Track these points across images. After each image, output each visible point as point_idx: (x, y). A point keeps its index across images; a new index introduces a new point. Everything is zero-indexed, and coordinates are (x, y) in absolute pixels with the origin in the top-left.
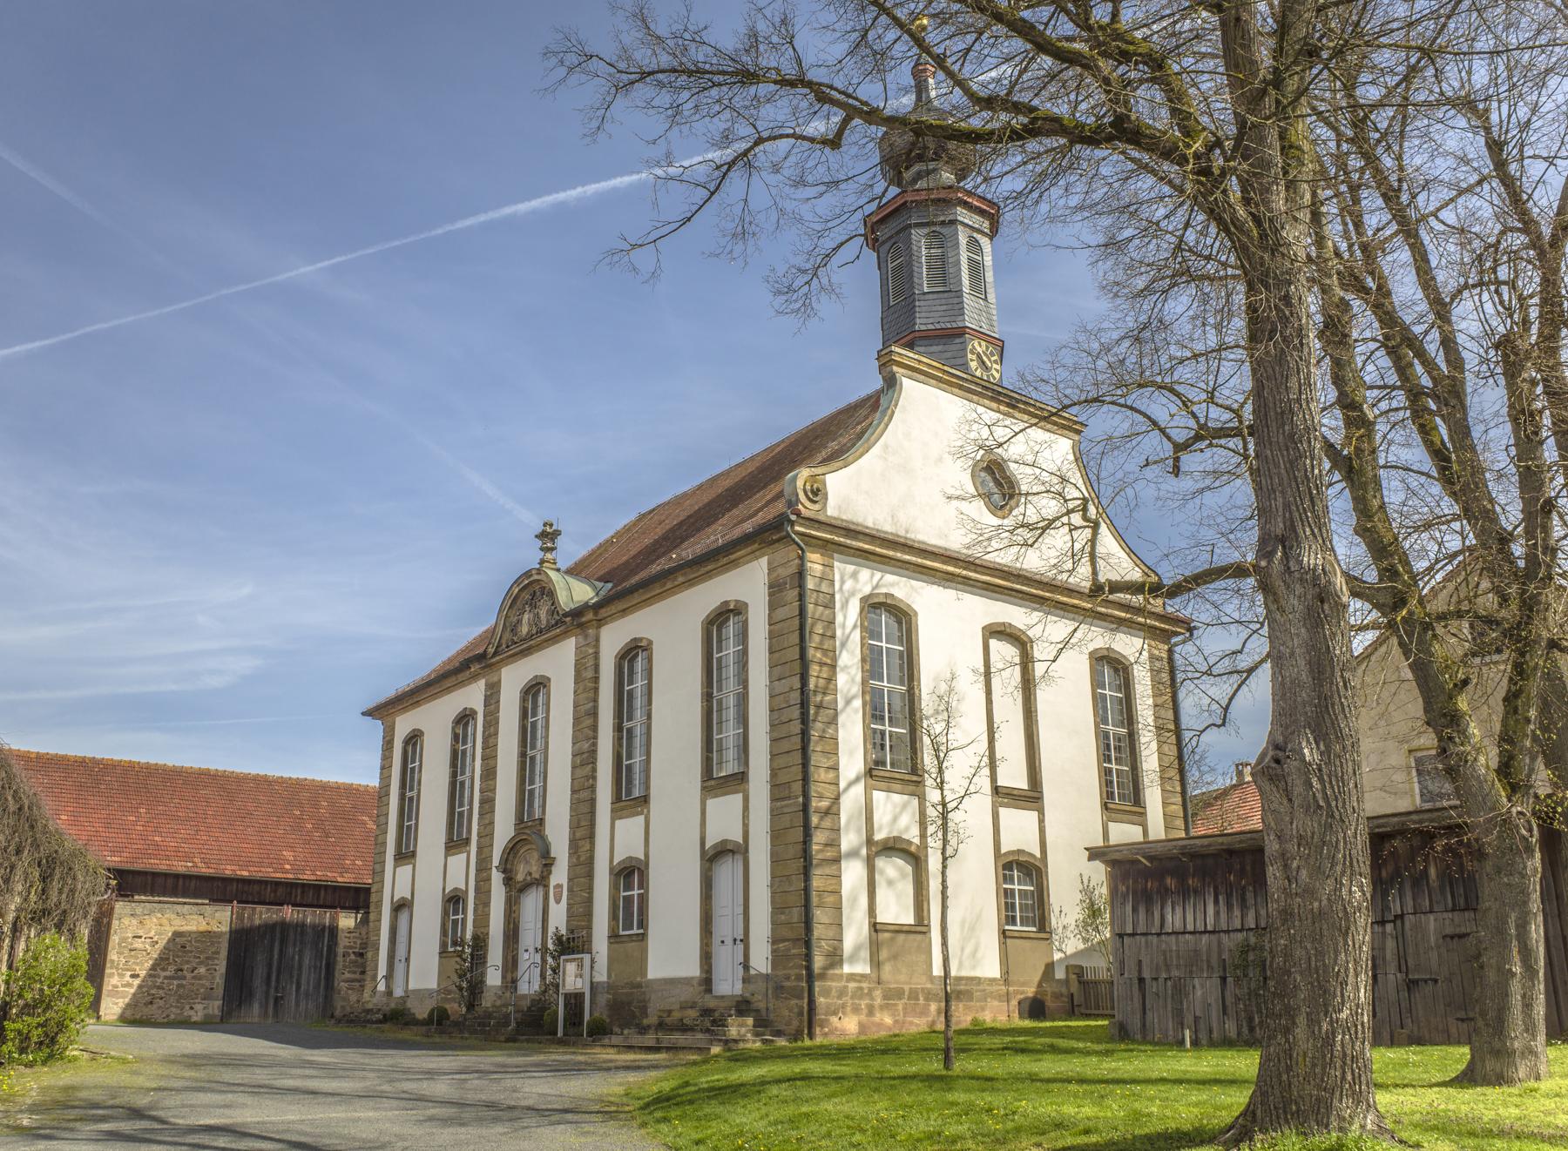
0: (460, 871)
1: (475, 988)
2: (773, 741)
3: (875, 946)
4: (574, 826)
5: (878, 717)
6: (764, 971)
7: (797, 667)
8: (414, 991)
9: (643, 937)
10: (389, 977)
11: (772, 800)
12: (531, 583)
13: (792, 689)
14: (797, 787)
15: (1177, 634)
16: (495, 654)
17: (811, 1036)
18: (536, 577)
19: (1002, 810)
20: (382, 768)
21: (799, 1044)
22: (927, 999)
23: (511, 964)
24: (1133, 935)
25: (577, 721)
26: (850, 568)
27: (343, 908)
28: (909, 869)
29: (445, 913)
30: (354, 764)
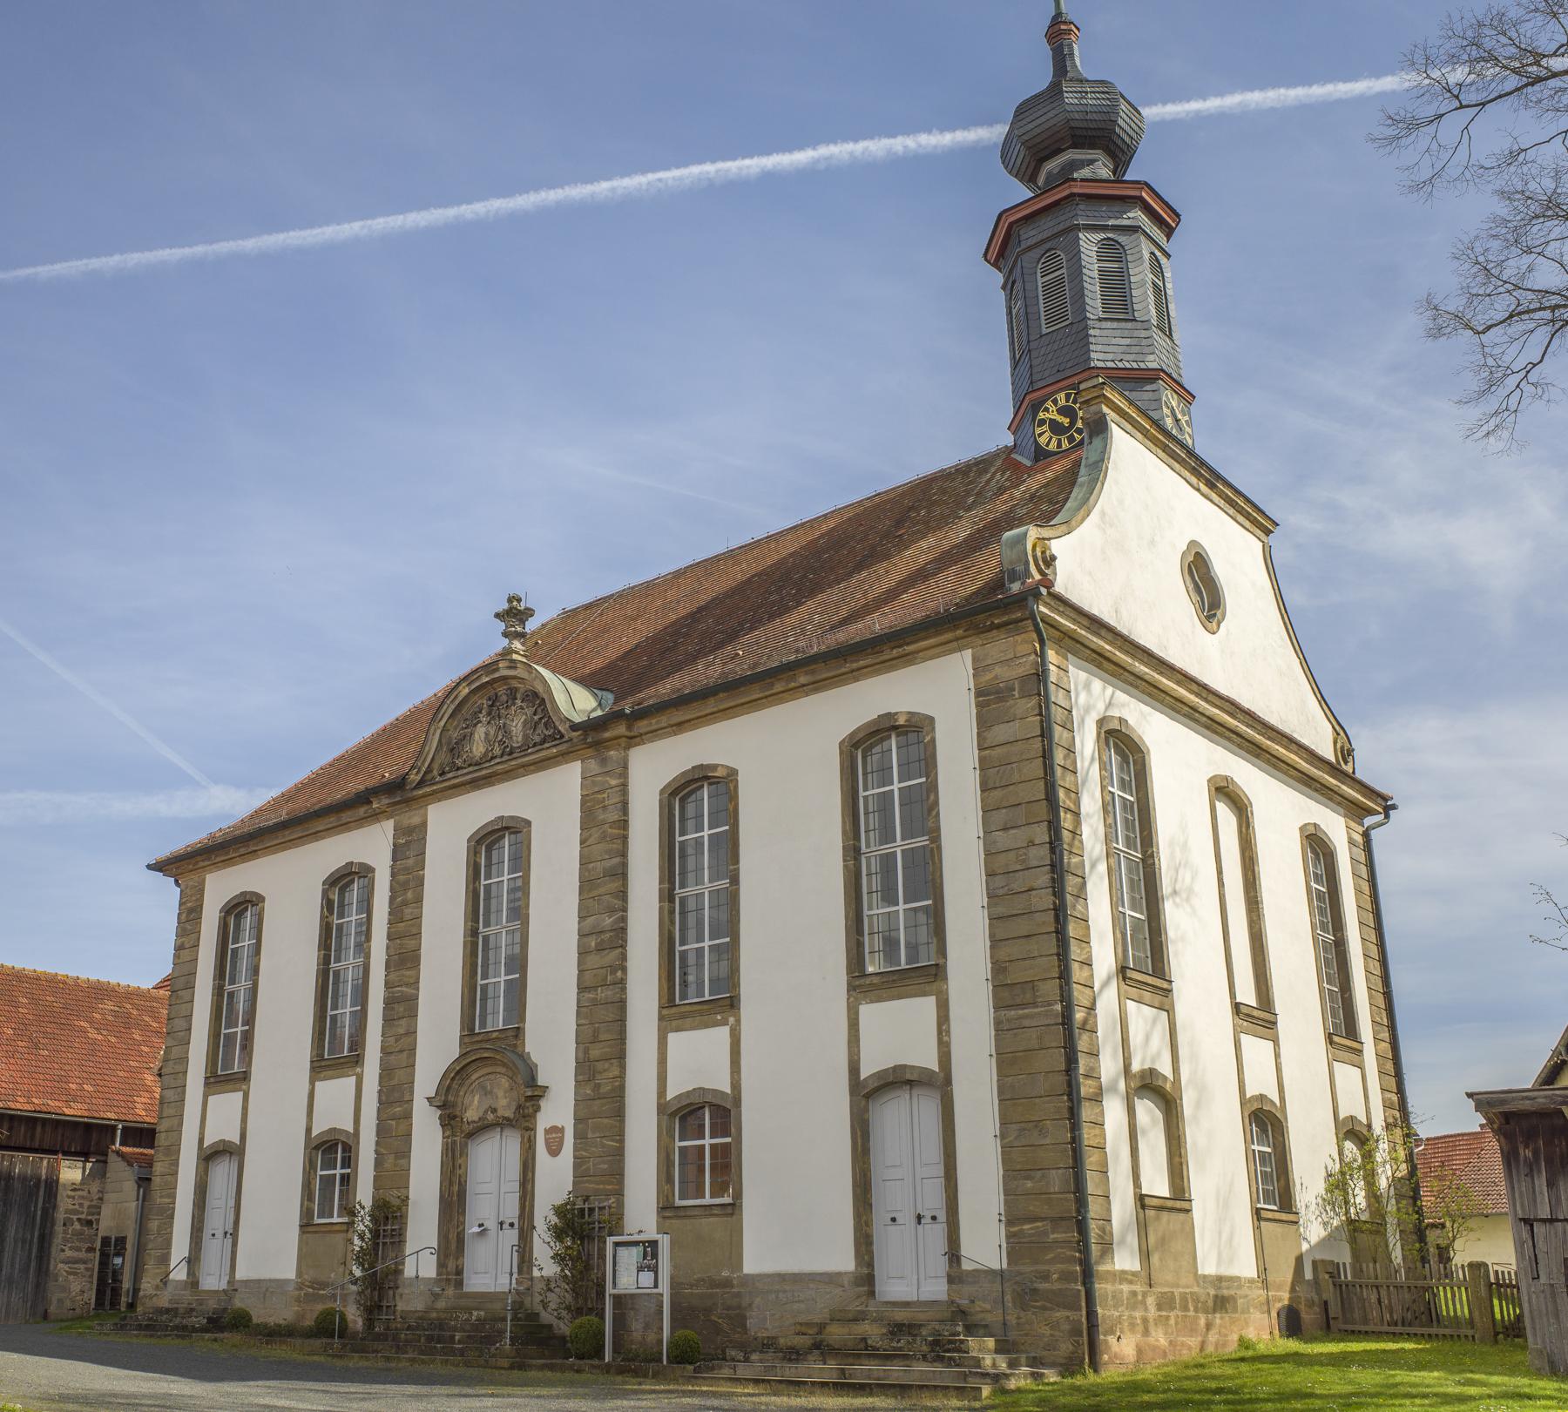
0: (342, 1103)
1: (380, 1283)
2: (994, 919)
3: (1143, 1227)
4: (586, 1039)
6: (996, 1266)
7: (1042, 810)
8: (246, 1283)
10: (193, 1260)
12: (494, 681)
13: (1031, 843)
14: (1051, 989)
15: (1371, 812)
17: (1095, 1366)
19: (935, 1066)
20: (179, 948)
21: (1078, 1380)
22: (1196, 1310)
23: (452, 1245)
24: (1552, 1221)
25: (586, 884)
26: (1083, 675)
27: (67, 1153)
28: (1159, 1115)
29: (310, 1167)
30: (123, 937)
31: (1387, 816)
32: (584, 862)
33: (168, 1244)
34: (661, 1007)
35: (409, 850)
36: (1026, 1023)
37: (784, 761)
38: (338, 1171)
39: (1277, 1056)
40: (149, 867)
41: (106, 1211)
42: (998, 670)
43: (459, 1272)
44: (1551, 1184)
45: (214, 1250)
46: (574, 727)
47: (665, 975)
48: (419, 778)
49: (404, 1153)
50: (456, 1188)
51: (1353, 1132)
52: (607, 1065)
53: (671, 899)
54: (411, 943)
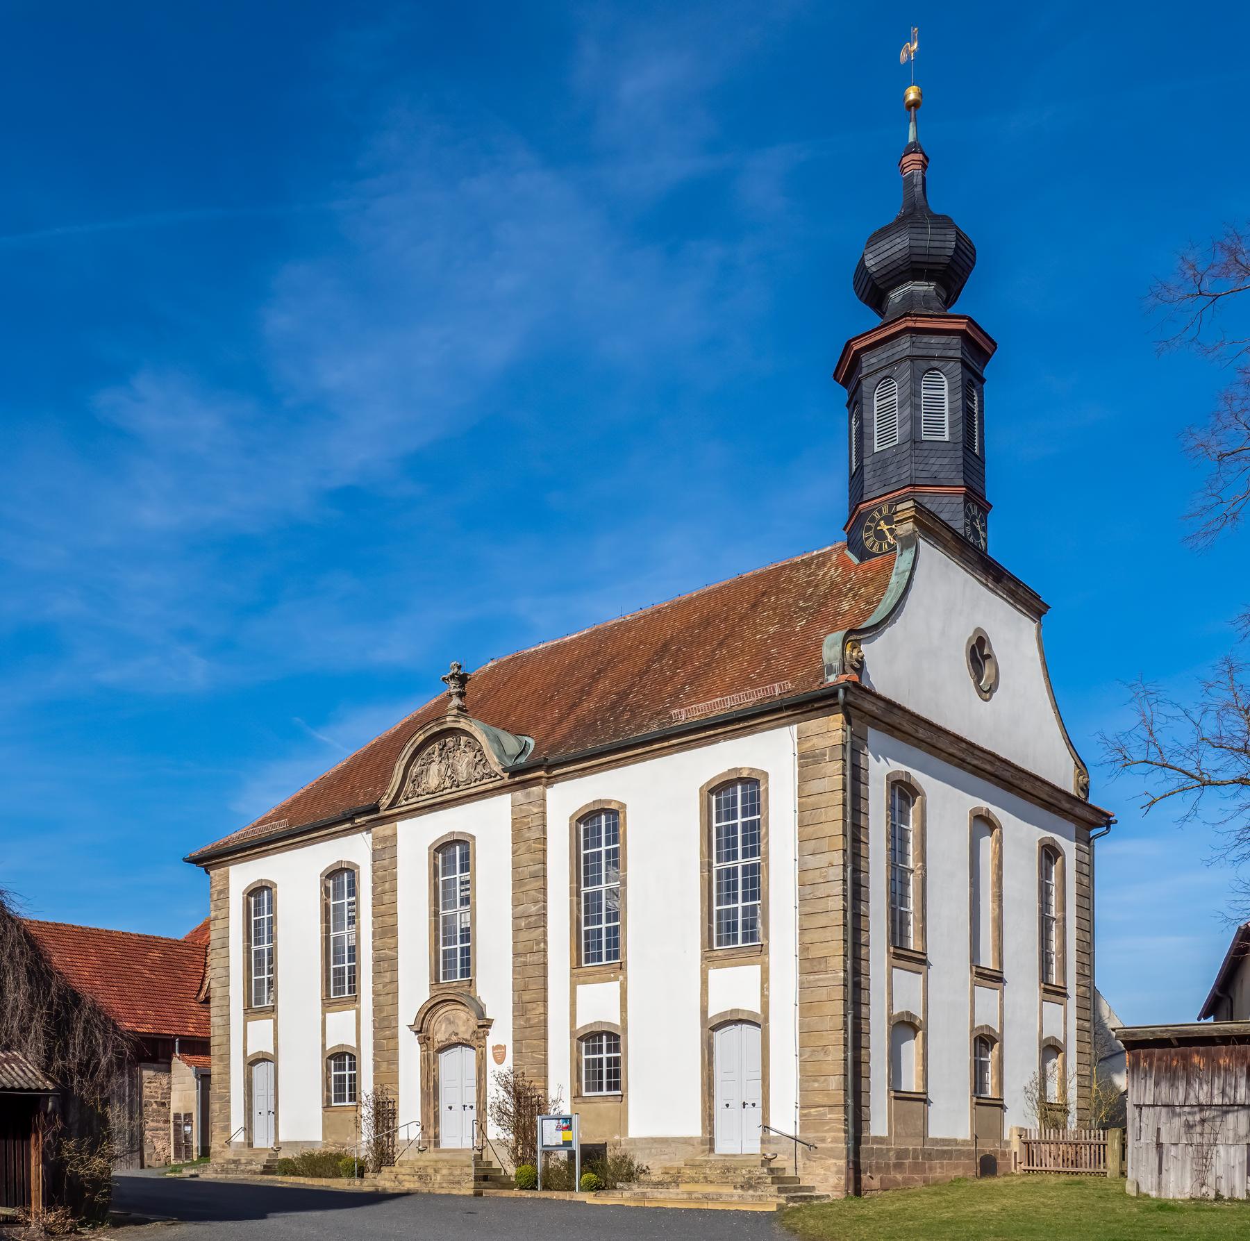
4: (520, 988)
8: (287, 1143)
10: (248, 1129)
16: (391, 806)
25: (517, 883)
31: (1108, 828)
32: (516, 867)
33: (228, 1119)
34: (572, 968)
35: (385, 856)
36: (820, 984)
38: (347, 1072)
39: (1002, 999)
40: (185, 860)
41: (174, 1096)
42: (815, 740)
43: (436, 1136)
44: (1157, 1084)
45: (259, 1123)
47: (575, 946)
48: (389, 802)
49: (394, 1061)
50: (432, 1084)
51: (1051, 1049)
52: (534, 1005)
53: (578, 895)
54: (389, 920)
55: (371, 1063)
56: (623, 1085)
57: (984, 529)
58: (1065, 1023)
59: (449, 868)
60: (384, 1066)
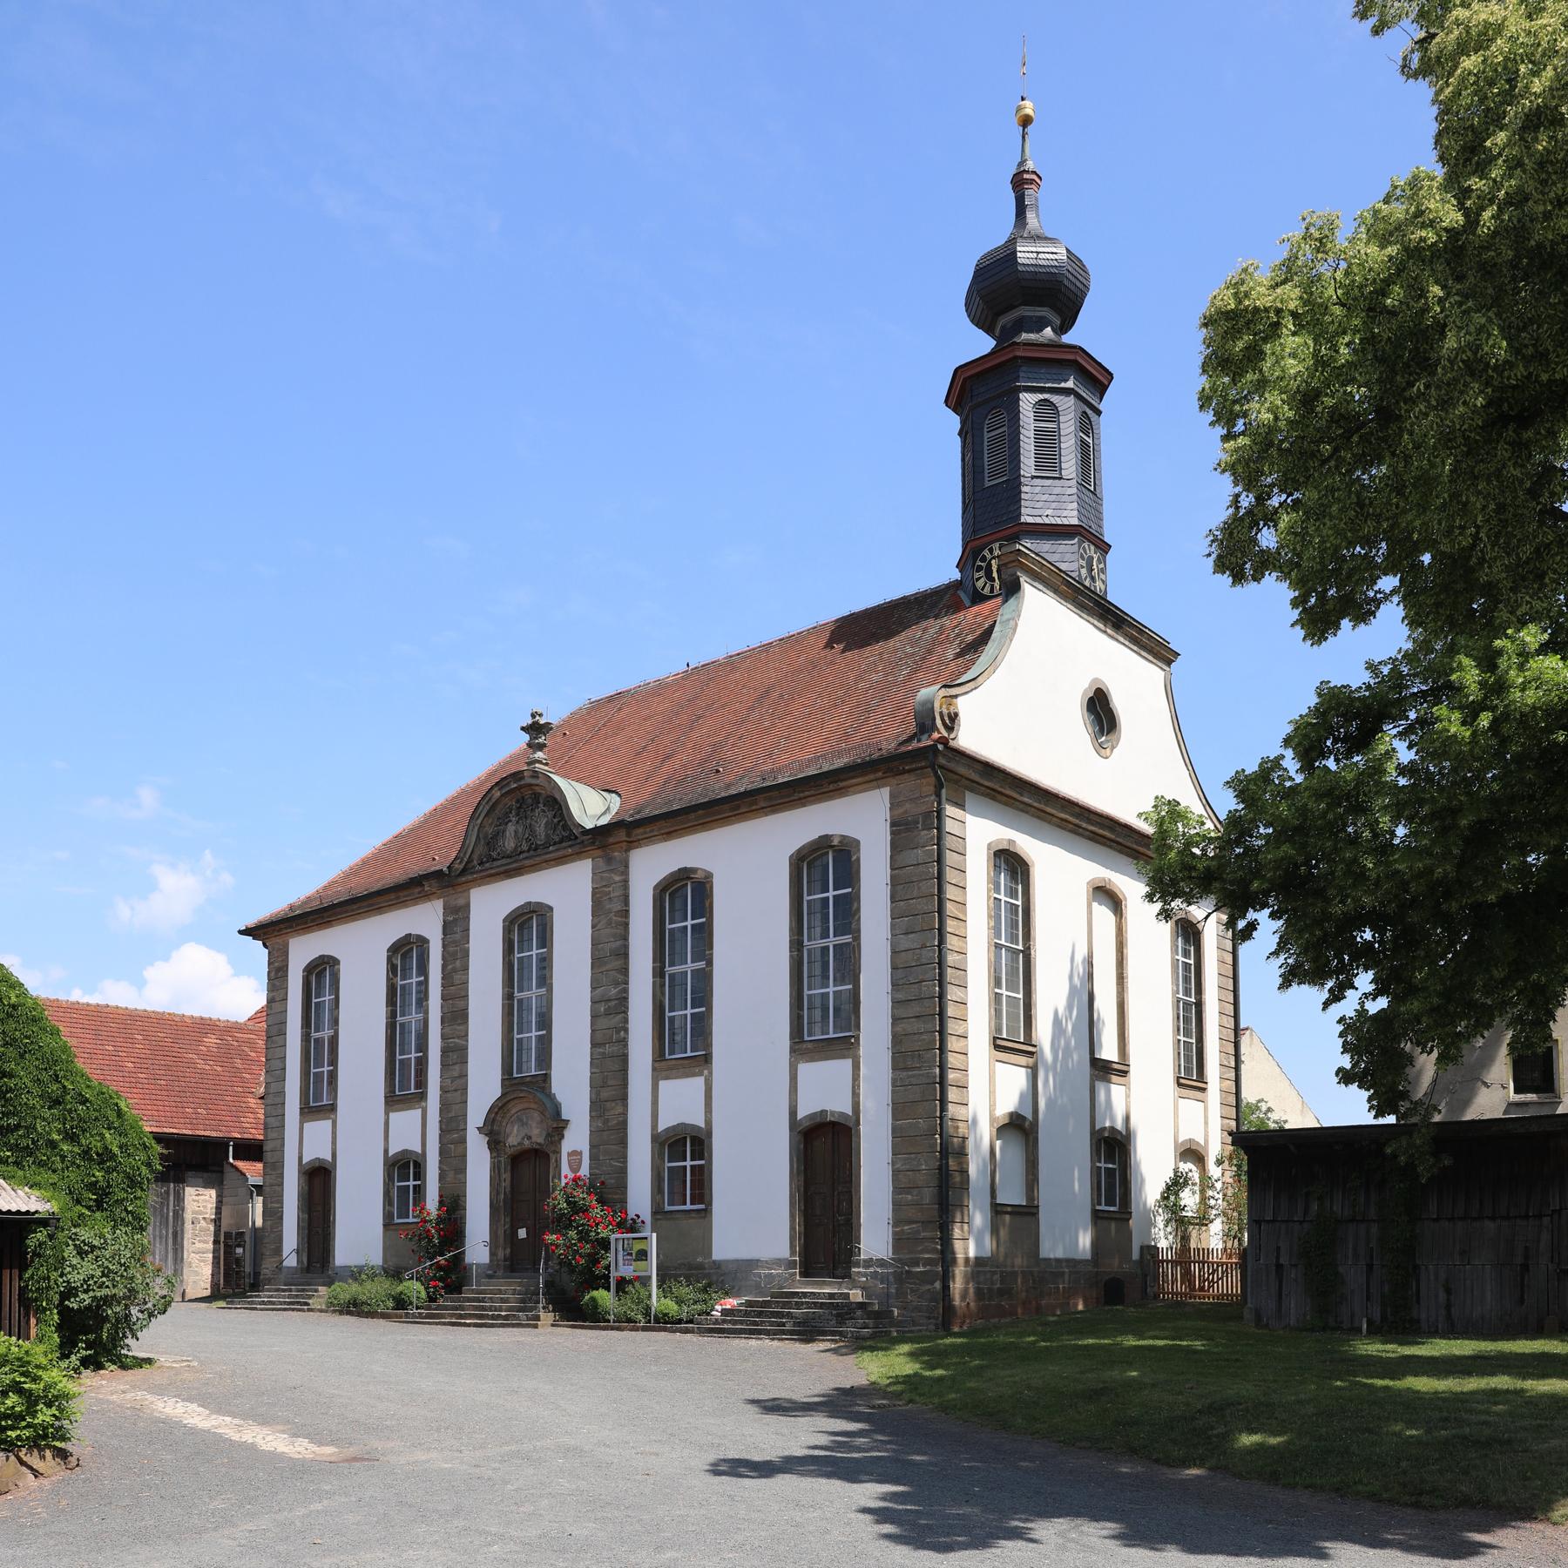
0: (412, 1130)
4: (597, 1085)
5: (998, 984)
9: (706, 1213)
11: (894, 1069)
18: (529, 781)
19: (702, 1125)
25: (597, 962)
35: (456, 926)
37: (748, 870)
40: (240, 932)
46: (586, 832)
49: (462, 1170)
54: (460, 1004)
55: (437, 1172)
56: (706, 1198)
57: (1103, 571)
58: (1206, 1123)
59: (525, 944)
60: (451, 1175)
